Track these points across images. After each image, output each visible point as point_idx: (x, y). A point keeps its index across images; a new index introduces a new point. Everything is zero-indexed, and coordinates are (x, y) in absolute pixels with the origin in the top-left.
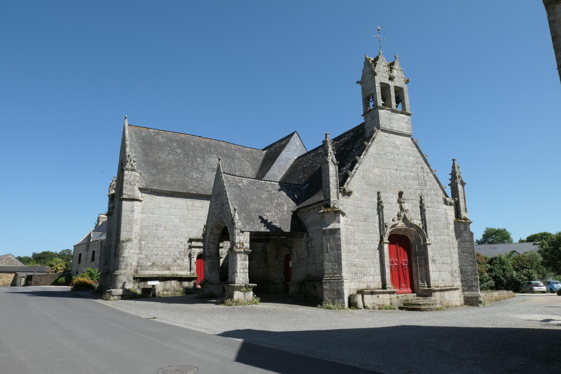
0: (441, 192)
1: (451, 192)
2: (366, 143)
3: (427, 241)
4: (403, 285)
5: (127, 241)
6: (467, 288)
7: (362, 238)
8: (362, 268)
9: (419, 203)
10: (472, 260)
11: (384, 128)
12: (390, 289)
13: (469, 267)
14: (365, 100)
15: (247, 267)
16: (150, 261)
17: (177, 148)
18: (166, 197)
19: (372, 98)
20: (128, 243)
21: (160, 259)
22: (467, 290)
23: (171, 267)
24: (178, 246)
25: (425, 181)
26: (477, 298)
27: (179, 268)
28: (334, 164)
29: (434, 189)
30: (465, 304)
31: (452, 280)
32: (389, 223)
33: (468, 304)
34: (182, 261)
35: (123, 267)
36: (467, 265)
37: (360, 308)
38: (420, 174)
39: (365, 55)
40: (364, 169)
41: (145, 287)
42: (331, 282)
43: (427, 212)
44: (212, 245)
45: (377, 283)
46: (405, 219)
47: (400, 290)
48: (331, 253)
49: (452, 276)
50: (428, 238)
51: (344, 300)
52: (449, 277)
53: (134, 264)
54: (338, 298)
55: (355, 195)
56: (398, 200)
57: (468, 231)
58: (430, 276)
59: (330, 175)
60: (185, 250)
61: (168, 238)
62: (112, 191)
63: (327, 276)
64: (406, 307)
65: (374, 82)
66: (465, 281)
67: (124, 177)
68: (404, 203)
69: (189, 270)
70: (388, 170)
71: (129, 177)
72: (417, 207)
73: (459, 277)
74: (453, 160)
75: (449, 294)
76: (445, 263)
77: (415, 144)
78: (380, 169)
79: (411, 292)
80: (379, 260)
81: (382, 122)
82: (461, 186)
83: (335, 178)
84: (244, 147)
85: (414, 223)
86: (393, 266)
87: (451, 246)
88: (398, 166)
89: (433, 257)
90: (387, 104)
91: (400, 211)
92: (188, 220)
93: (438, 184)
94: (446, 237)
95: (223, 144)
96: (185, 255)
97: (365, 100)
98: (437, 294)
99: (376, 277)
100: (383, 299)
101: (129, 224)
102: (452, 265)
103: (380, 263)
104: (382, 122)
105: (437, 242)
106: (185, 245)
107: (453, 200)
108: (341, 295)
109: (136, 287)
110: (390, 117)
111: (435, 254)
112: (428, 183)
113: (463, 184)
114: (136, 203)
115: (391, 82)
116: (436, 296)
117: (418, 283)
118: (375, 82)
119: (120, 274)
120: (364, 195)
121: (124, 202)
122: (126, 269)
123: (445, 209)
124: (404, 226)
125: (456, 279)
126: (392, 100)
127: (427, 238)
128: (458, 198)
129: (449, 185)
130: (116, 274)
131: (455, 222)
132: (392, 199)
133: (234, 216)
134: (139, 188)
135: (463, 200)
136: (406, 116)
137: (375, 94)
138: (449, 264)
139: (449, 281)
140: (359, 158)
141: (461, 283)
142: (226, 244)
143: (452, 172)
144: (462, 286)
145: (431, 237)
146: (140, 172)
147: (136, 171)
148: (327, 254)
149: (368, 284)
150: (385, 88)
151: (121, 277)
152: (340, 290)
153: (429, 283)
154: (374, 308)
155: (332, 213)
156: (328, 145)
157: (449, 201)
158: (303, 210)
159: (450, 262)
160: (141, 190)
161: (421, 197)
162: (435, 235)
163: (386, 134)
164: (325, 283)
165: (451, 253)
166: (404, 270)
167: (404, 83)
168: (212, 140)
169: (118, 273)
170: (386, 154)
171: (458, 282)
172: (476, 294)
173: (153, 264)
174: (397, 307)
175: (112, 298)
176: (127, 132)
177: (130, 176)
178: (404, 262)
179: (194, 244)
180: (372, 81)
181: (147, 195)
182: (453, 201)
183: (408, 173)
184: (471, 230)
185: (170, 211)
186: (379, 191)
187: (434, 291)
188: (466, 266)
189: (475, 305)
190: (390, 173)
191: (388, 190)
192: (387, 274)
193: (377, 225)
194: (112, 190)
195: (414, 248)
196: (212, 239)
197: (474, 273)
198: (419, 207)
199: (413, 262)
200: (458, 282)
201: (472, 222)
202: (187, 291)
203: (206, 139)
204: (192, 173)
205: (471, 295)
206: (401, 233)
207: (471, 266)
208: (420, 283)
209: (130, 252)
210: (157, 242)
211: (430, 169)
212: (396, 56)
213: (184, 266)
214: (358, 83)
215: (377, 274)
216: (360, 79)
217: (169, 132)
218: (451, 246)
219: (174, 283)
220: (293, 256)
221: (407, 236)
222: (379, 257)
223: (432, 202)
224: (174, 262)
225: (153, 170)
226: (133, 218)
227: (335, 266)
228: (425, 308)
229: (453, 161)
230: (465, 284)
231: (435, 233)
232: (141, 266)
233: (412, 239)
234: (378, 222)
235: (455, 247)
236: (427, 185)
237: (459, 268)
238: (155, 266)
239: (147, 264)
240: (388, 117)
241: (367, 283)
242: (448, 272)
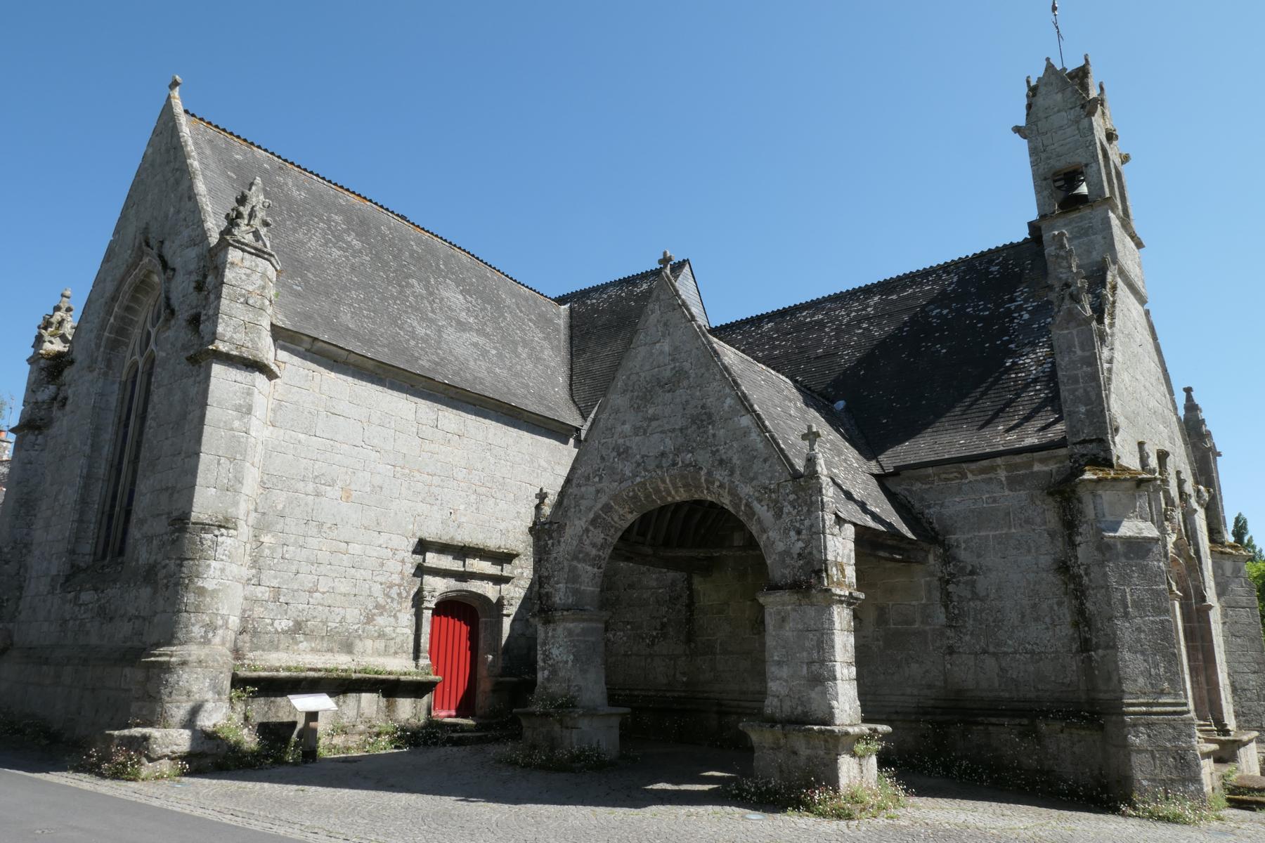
5: (220, 526)
13: (1251, 676)
14: (1045, 179)
17: (347, 231)
18: (356, 381)
20: (222, 535)
21: (320, 608)
23: (357, 641)
24: (382, 565)
27: (380, 644)
34: (392, 619)
35: (197, 631)
41: (271, 720)
42: (1153, 724)
44: (589, 568)
48: (1138, 620)
53: (234, 622)
54: (1184, 781)
57: (1243, 580)
60: (402, 579)
61: (354, 529)
62: (51, 342)
63: (1134, 701)
66: (1244, 715)
67: (227, 270)
69: (411, 656)
71: (244, 277)
92: (416, 474)
96: (402, 598)
101: (232, 459)
108: (1189, 768)
109: (237, 718)
114: (259, 378)
119: (184, 663)
121: (217, 369)
122: (206, 641)
130: (161, 663)
134: (272, 325)
137: (1093, 165)
142: (520, 570)
146: (278, 268)
147: (272, 259)
148: (1127, 625)
151: (185, 676)
152: (1186, 750)
155: (1128, 484)
158: (930, 470)
160: (281, 336)
169: (173, 659)
173: (298, 627)
175: (147, 769)
177: (248, 271)
179: (432, 559)
180: (1078, 129)
181: (296, 360)
185: (367, 434)
194: (52, 339)
196: (594, 545)
202: (413, 738)
204: (409, 320)
207: (1256, 675)
209: (227, 572)
210: (316, 541)
213: (398, 640)
217: (315, 177)
219: (370, 702)
224: (368, 623)
225: (292, 278)
226: (247, 438)
227: (1156, 666)
229: (1185, 394)
230: (1245, 721)
232: (255, 633)
238: (304, 634)
239: (276, 623)
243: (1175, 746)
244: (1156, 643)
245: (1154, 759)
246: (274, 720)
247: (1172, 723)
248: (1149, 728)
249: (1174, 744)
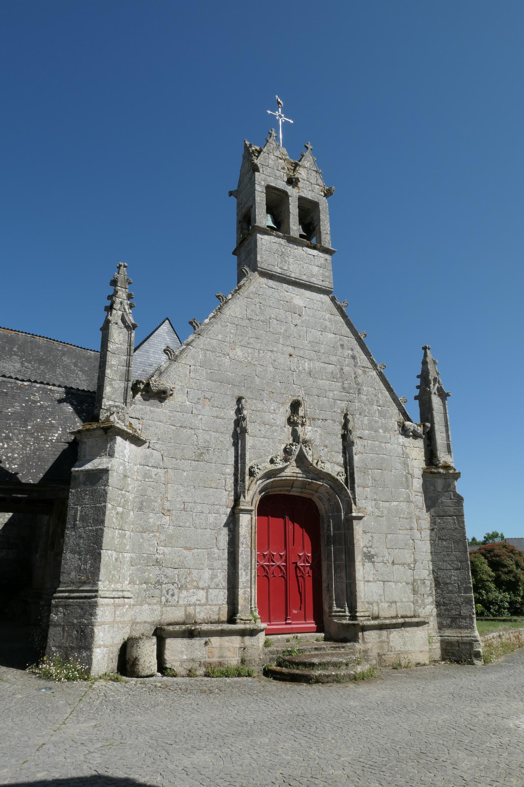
0: (395, 410)
1: (419, 412)
3: (353, 511)
4: (295, 612)
6: (449, 621)
7: (186, 499)
8: (176, 571)
9: (340, 427)
10: (460, 557)
11: (266, 269)
12: (245, 623)
13: (454, 572)
22: (450, 627)
25: (358, 384)
26: (471, 643)
29: (378, 401)
30: (443, 659)
31: (415, 602)
32: (259, 467)
33: (450, 659)
36: (449, 567)
37: (143, 674)
38: (346, 369)
39: (244, 141)
40: (209, 347)
42: (69, 605)
43: (355, 449)
45: (216, 609)
46: (301, 460)
47: (286, 624)
49: (415, 592)
50: (355, 504)
51: (91, 655)
52: (406, 595)
54: (80, 649)
56: (289, 419)
58: (356, 591)
63: (64, 589)
64: (284, 670)
66: (445, 604)
68: (303, 425)
70: (269, 353)
72: (334, 437)
73: (430, 595)
75: (402, 635)
76: (400, 562)
78: (250, 350)
79: (315, 630)
80: (226, 551)
81: (262, 258)
82: (439, 399)
83: (125, 358)
84: (84, 349)
85: (324, 470)
86: (273, 567)
87: (415, 525)
88: (294, 348)
89: (369, 549)
91: (291, 442)
93: (387, 393)
94: (404, 505)
95: (41, 341)
97: (240, 222)
98: (371, 636)
99: (213, 593)
100: (221, 648)
102: (414, 567)
103: (228, 559)
104: (262, 258)
105: (380, 514)
107: (420, 426)
108: (85, 639)
110: (284, 250)
111: (374, 541)
112: (365, 388)
115: (291, 187)
116: (368, 641)
117: (331, 607)
118: (255, 184)
120: (200, 401)
123: (404, 446)
124: (301, 475)
125: (423, 601)
126: (291, 220)
127: (353, 505)
128: (433, 424)
129: (416, 398)
131: (425, 474)
132: (275, 415)
135: (443, 429)
136: (320, 254)
137: (253, 206)
138: (409, 565)
139: (407, 604)
141: (435, 610)
143: (423, 371)
144: (439, 615)
148: (73, 533)
149: (191, 610)
152: (86, 625)
153: (353, 609)
154: (190, 674)
157: (412, 429)
159: (410, 560)
161: (346, 415)
162: (375, 500)
163: (271, 283)
164: (57, 606)
165: (413, 540)
166: (301, 576)
167: (323, 194)
168: (20, 334)
170: (267, 322)
171: (428, 607)
172: (469, 635)
174: (257, 669)
178: (302, 558)
182: (420, 430)
183: (318, 365)
184: (458, 491)
186: (241, 395)
187: (364, 629)
188: (446, 570)
189: (465, 661)
190: (274, 361)
191: (265, 395)
192: (241, 585)
193: (230, 470)
197: (464, 586)
198: (340, 436)
199: (323, 558)
200: (428, 607)
203: (8, 331)
205: (458, 638)
206: (295, 492)
208: (335, 608)
211: (372, 360)
214: (231, 195)
215: (218, 585)
216: (235, 188)
218: (415, 525)
221: (312, 498)
222: (226, 544)
223: (371, 428)
227: (86, 563)
228: (320, 675)
230: (445, 610)
231: (377, 494)
233: (322, 507)
234: (233, 462)
235: (424, 527)
237: (431, 576)
240: (277, 250)
241: (186, 608)
242: (404, 583)
243: (80, 622)
244: (89, 546)
245: (63, 632)
247: (81, 605)
248: (66, 608)
249: (79, 621)
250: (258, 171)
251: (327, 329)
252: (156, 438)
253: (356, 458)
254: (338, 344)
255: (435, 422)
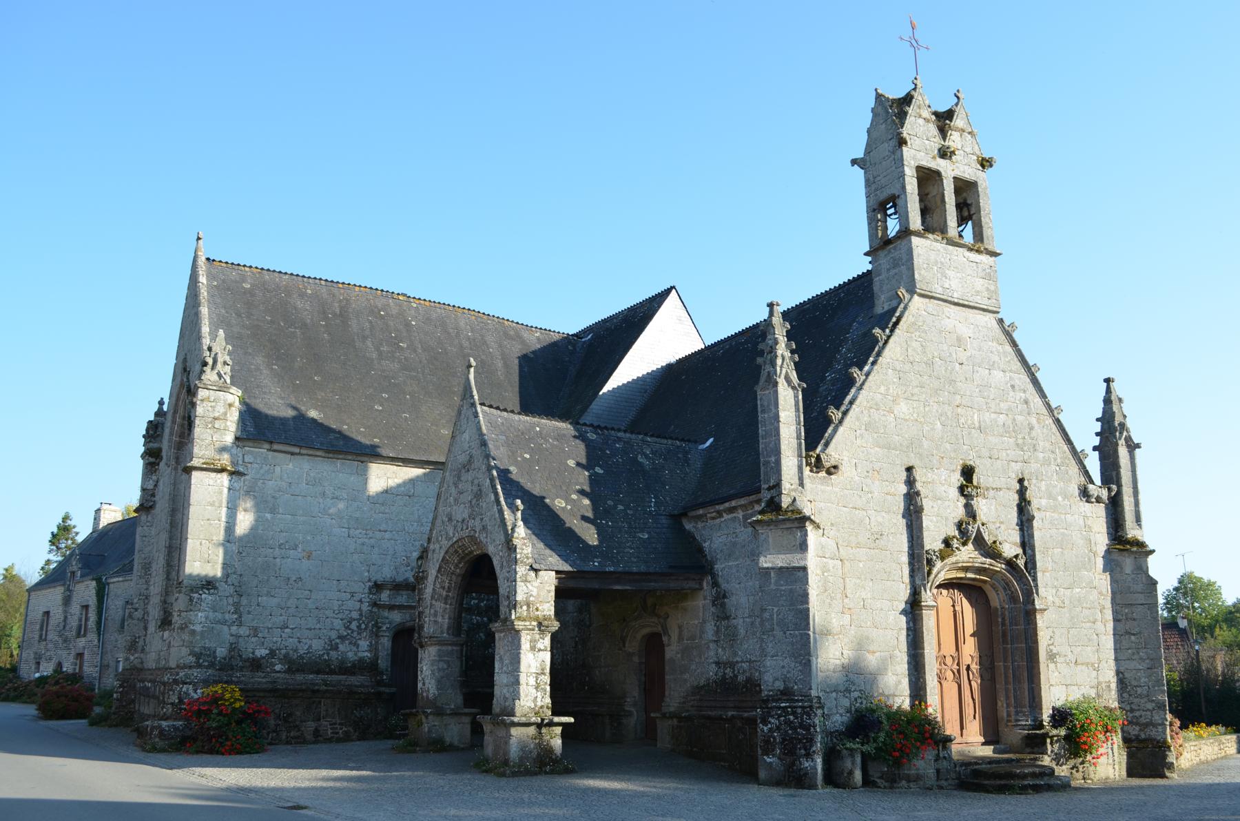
0: (1074, 469)
2: (877, 331)
15: (548, 670)
16: (263, 643)
19: (894, 206)
28: (794, 388)
29: (1055, 459)
55: (846, 471)
59: (781, 419)
60: (361, 615)
65: (900, 162)
71: (210, 408)
74: (1108, 381)
77: (1008, 335)
81: (920, 274)
89: (1051, 647)
90: (933, 223)
104: (920, 274)
106: (361, 601)
113: (1132, 447)
118: (903, 165)
128: (1119, 486)
129: (1095, 449)
133: (513, 529)
137: (902, 196)
138: (1093, 665)
140: (859, 373)
143: (1104, 412)
145: (1048, 593)
150: (928, 177)
156: (777, 336)
165: (1097, 635)
176: (203, 279)
182: (1104, 494)
184: (1152, 573)
195: (1000, 620)
201: (1154, 551)
212: (959, 95)
216: (860, 154)
220: (669, 640)
236: (1037, 448)
246: (759, 764)
250: (906, 143)
251: (996, 365)
252: (829, 524)
253: (1037, 534)
254: (1009, 385)
255: (1123, 483)
